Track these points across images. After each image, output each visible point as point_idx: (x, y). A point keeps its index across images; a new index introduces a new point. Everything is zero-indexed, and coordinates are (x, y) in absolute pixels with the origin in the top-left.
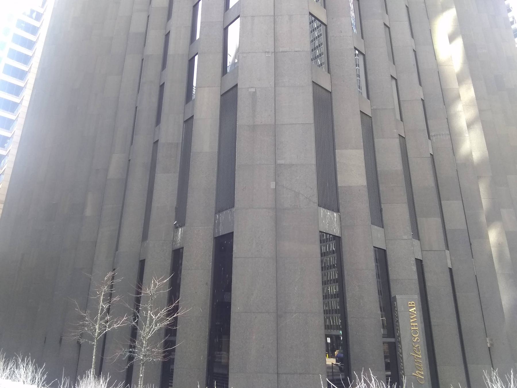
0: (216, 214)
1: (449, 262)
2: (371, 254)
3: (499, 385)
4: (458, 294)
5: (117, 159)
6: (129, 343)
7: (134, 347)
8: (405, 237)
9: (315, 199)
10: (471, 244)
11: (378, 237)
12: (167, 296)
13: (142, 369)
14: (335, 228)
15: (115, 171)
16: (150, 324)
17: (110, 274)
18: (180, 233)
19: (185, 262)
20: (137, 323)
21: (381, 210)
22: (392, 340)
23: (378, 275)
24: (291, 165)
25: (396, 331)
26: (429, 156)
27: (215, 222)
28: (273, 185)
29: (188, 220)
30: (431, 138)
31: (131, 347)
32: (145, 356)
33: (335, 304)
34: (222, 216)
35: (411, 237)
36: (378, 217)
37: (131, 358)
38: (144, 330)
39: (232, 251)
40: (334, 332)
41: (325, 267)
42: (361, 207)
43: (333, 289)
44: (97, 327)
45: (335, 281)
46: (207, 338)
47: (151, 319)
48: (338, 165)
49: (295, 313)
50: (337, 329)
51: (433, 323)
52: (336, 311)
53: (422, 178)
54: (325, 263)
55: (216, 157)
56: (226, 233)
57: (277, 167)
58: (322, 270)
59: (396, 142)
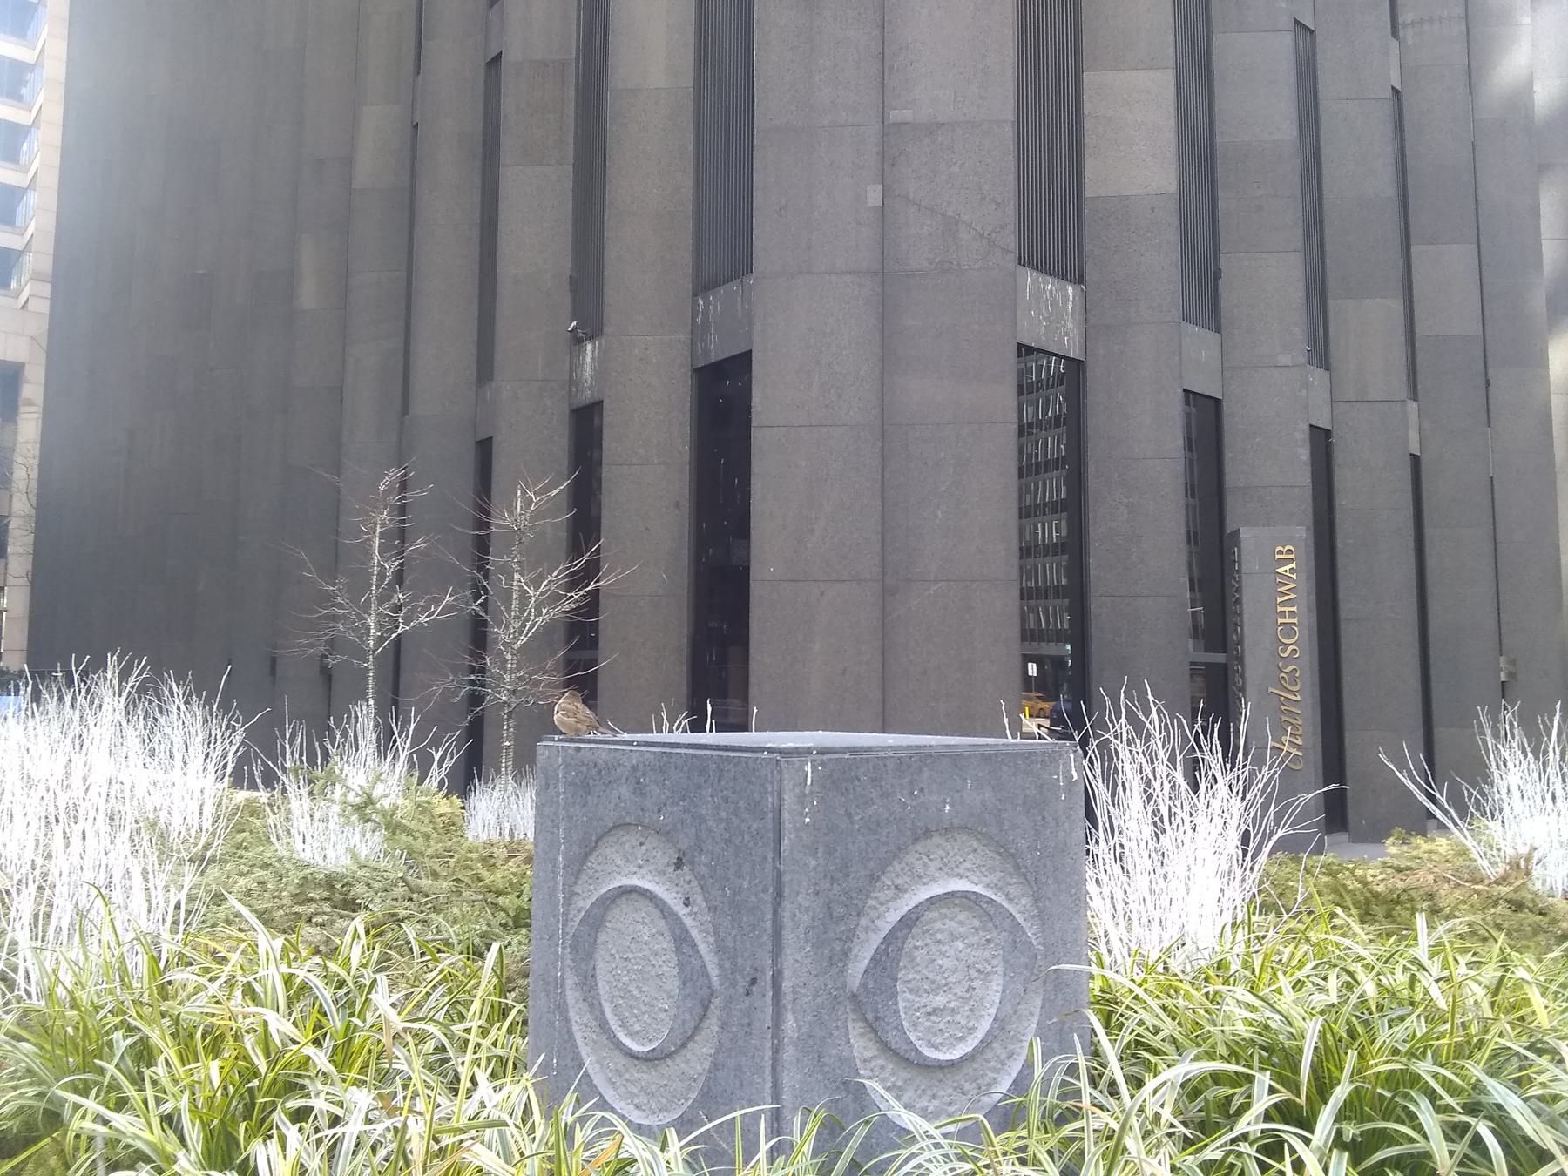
0: (695, 294)
1: (1413, 436)
2: (1175, 410)
3: (1515, 745)
4: (1429, 531)
5: (377, 124)
6: (467, 660)
7: (483, 671)
8: (1285, 359)
9: (1010, 240)
10: (1488, 383)
11: (1200, 361)
12: (563, 535)
13: (508, 728)
14: (1067, 334)
15: (372, 162)
16: (522, 611)
17: (393, 474)
18: (588, 359)
19: (611, 445)
20: (484, 605)
21: (1217, 277)
22: (1220, 658)
23: (1190, 440)
24: (933, 128)
25: (1230, 628)
26: (1389, 93)
27: (694, 322)
28: (874, 196)
29: (612, 319)
30: (1401, 33)
31: (472, 670)
32: (514, 692)
33: (1053, 571)
34: (715, 302)
35: (1303, 360)
36: (1204, 300)
37: (475, 699)
38: (507, 627)
39: (750, 407)
40: (1050, 649)
41: (1029, 466)
42: (1152, 262)
43: (1052, 530)
44: (371, 621)
45: (1057, 507)
46: (685, 652)
47: (524, 597)
48: (1087, 125)
49: (936, 581)
50: (1058, 641)
51: (1343, 614)
52: (1058, 592)
53: (1359, 167)
54: (1030, 457)
55: (690, 105)
56: (727, 355)
57: (890, 132)
58: (1021, 476)
59: (1286, 42)
